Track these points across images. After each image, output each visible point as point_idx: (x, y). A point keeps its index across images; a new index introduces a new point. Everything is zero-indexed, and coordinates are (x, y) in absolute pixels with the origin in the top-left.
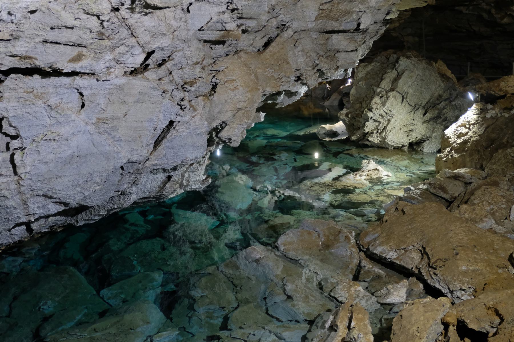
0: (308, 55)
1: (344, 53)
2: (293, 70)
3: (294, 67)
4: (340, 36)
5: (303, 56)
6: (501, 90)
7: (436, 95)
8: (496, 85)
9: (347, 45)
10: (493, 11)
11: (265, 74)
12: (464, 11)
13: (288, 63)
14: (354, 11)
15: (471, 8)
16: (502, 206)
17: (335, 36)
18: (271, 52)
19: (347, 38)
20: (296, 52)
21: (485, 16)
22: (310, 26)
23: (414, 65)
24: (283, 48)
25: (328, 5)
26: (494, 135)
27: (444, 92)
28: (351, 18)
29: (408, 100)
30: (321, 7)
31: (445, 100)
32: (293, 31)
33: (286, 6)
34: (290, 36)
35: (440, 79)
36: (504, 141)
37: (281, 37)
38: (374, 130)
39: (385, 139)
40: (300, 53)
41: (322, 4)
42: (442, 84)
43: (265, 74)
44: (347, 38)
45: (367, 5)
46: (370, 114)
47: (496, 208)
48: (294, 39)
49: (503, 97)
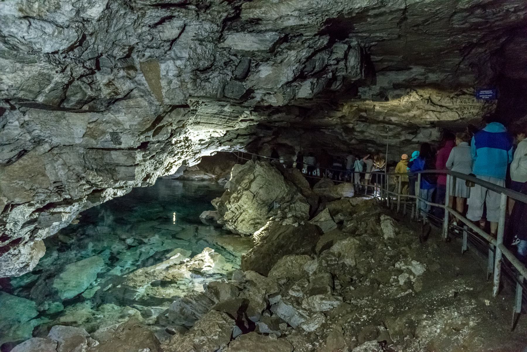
0: (71, 168)
1: (124, 168)
2: (52, 182)
3: (53, 179)
4: (118, 153)
5: (64, 169)
6: (337, 194)
7: (280, 197)
8: (335, 189)
9: (126, 161)
10: (344, 134)
11: (12, 185)
12: (326, 133)
13: (44, 175)
14: (108, 132)
15: (330, 130)
16: (214, 337)
17: (112, 152)
18: (20, 164)
19: (125, 154)
20: (56, 165)
21: (340, 137)
22: (77, 142)
23: (265, 172)
24: (38, 162)
25: (94, 124)
26: (283, 242)
27: (287, 195)
28: (105, 138)
29: (257, 198)
30: (88, 126)
31: (288, 202)
32: (50, 146)
33: (45, 122)
34: (47, 151)
35: (284, 185)
36: (290, 248)
37: (36, 151)
38: (230, 219)
39: (237, 227)
40: (60, 167)
41: (89, 123)
42: (286, 189)
43: (12, 185)
44: (125, 154)
45: (121, 127)
46: (228, 206)
47: (205, 340)
48: (53, 154)
49: (339, 199)
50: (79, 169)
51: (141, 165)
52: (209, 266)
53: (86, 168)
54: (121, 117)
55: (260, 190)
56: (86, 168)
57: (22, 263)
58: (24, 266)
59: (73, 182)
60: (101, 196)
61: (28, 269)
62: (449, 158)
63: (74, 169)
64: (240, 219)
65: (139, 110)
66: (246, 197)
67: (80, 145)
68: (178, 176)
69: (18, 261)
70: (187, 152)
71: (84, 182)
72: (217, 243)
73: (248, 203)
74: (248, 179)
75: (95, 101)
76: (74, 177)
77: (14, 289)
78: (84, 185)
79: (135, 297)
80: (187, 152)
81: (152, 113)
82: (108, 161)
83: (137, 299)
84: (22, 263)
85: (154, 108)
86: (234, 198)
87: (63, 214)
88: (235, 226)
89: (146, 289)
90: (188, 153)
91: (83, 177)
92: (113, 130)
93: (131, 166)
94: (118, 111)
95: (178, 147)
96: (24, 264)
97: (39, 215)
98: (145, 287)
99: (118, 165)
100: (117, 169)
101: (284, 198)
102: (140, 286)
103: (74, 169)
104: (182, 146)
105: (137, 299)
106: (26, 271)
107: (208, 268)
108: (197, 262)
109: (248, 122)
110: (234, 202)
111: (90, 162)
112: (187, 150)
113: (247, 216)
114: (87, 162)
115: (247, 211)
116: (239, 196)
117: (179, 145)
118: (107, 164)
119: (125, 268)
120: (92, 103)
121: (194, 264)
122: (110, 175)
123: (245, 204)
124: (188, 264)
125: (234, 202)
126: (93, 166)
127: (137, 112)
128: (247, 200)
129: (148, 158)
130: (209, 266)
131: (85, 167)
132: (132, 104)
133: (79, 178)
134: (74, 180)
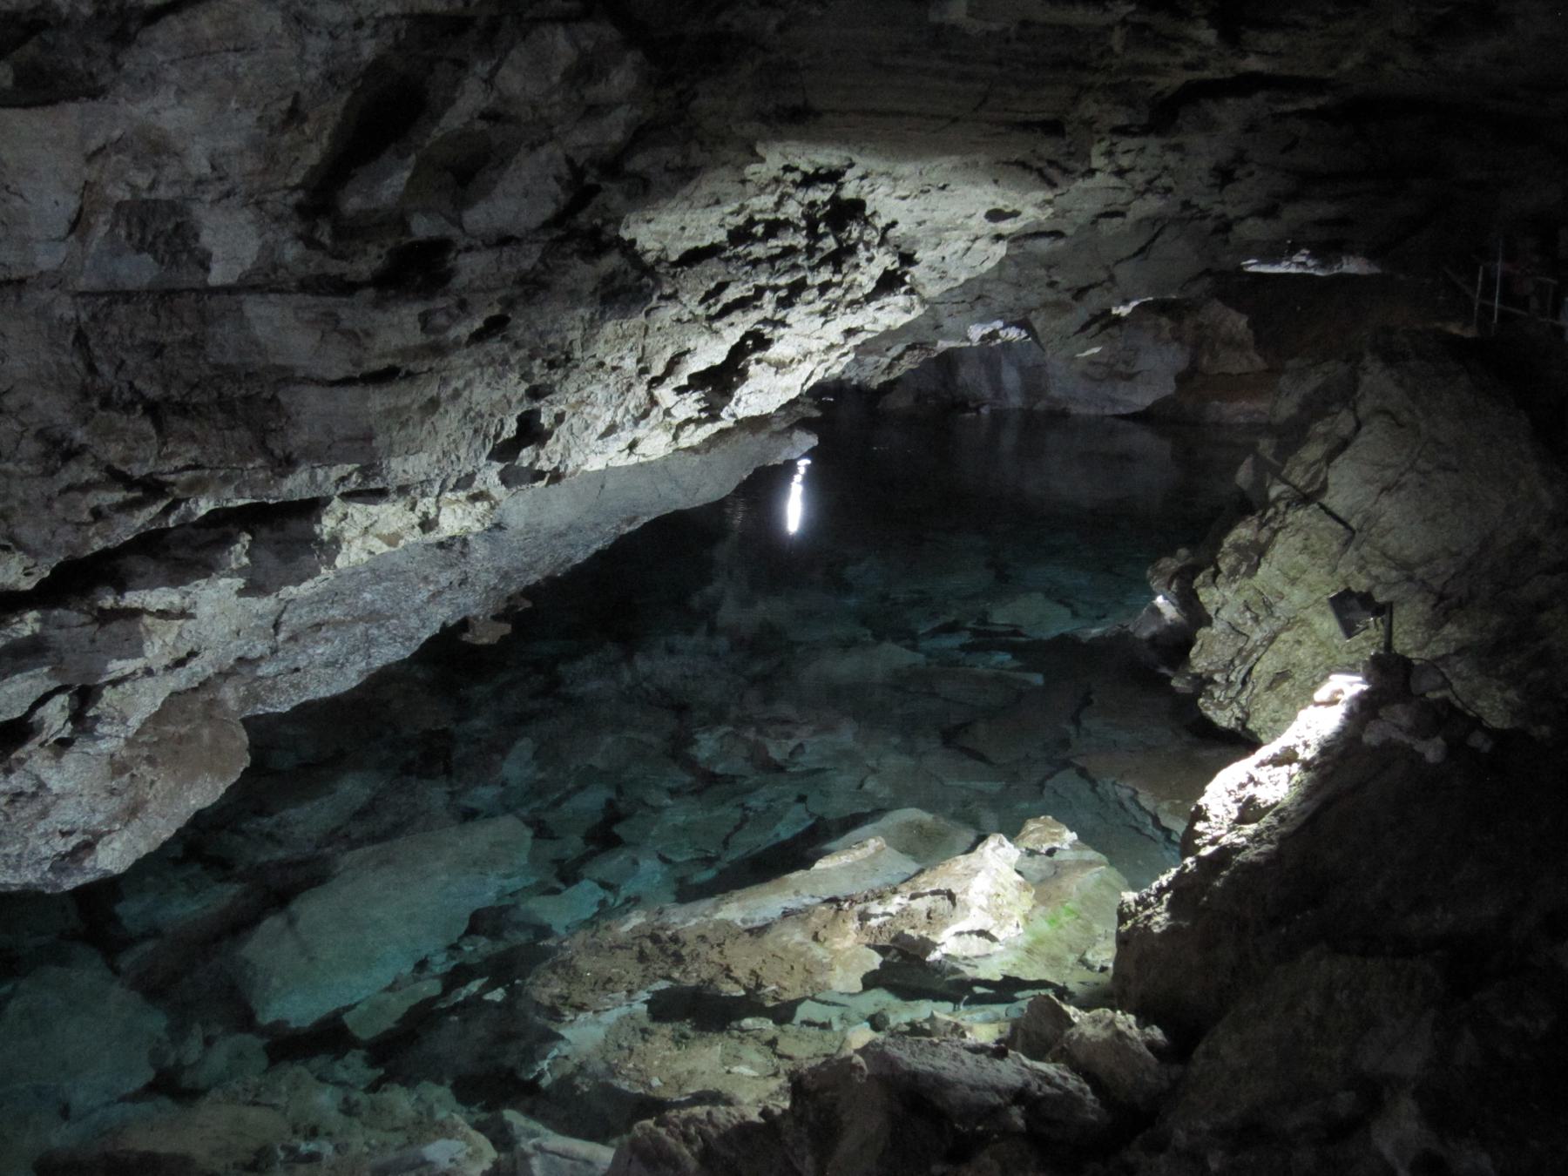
19: (307, 315)
22: (47, 259)
29: (1366, 549)
41: (90, 158)
42: (1544, 494)
44: (307, 315)
50: (54, 409)
51: (410, 375)
52: (982, 933)
53: (95, 398)
54: (171, 114)
55: (1385, 501)
56: (95, 398)
57: (64, 834)
58: (77, 849)
59: (26, 476)
60: (315, 538)
61: (87, 863)
62: (706, 436)
63: (26, 406)
64: (1267, 665)
65: (242, 64)
66: (1297, 541)
67: (57, 280)
68: (1148, 401)
69: (41, 827)
70: (824, 287)
71: (90, 474)
72: (1134, 799)
73: (1312, 577)
74: (1325, 437)
75: (48, 37)
76: (32, 448)
77: (128, 943)
78: (87, 487)
79: (545, 1064)
80: (824, 287)
81: (313, 74)
82: (231, 358)
83: (545, 1082)
84: (64, 834)
85: (318, 45)
86: (1237, 547)
87: (148, 620)
88: (1242, 708)
89: (613, 1031)
90: (834, 293)
91: (83, 448)
92: (133, 188)
93: (347, 382)
94: (150, 82)
95: (756, 263)
96: (74, 841)
97: (43, 621)
98: (610, 1017)
99: (286, 377)
100: (283, 397)
101: (1535, 545)
102: (581, 1008)
103: (26, 406)
104: (789, 251)
105: (545, 1082)
106: (81, 870)
107: (976, 946)
108: (921, 905)
109: (1260, 97)
110: (1234, 572)
111: (121, 365)
112: (825, 275)
113: (1301, 653)
114: (105, 368)
115: (1304, 622)
116: (1265, 534)
117: (758, 250)
118: (227, 372)
119: (623, 893)
120: (31, 49)
121: (905, 913)
122: (243, 435)
123: (1293, 582)
124: (875, 908)
125: (1234, 572)
126: (138, 383)
127: (234, 77)
128: (1303, 560)
129: (462, 330)
130: (982, 933)
131: (85, 394)
132: (209, 32)
133: (60, 451)
134: (31, 462)
